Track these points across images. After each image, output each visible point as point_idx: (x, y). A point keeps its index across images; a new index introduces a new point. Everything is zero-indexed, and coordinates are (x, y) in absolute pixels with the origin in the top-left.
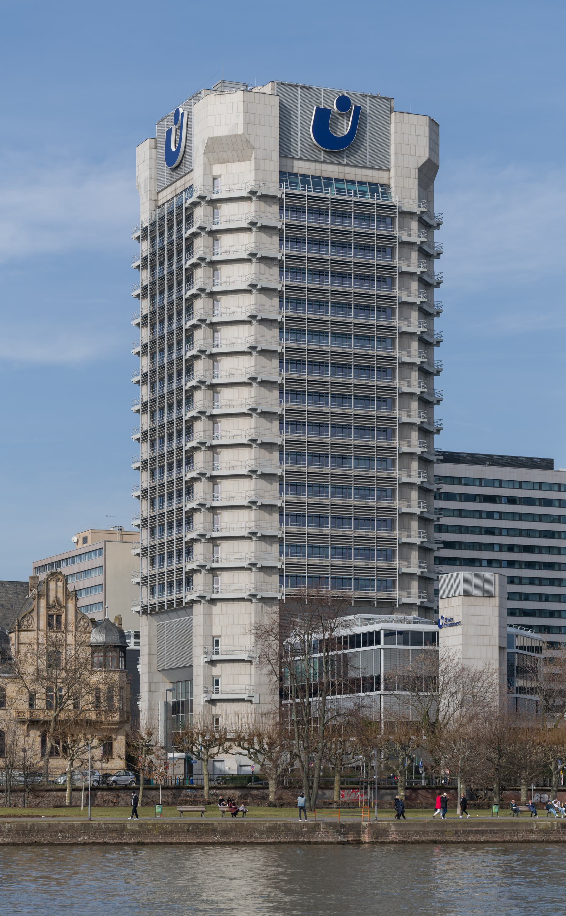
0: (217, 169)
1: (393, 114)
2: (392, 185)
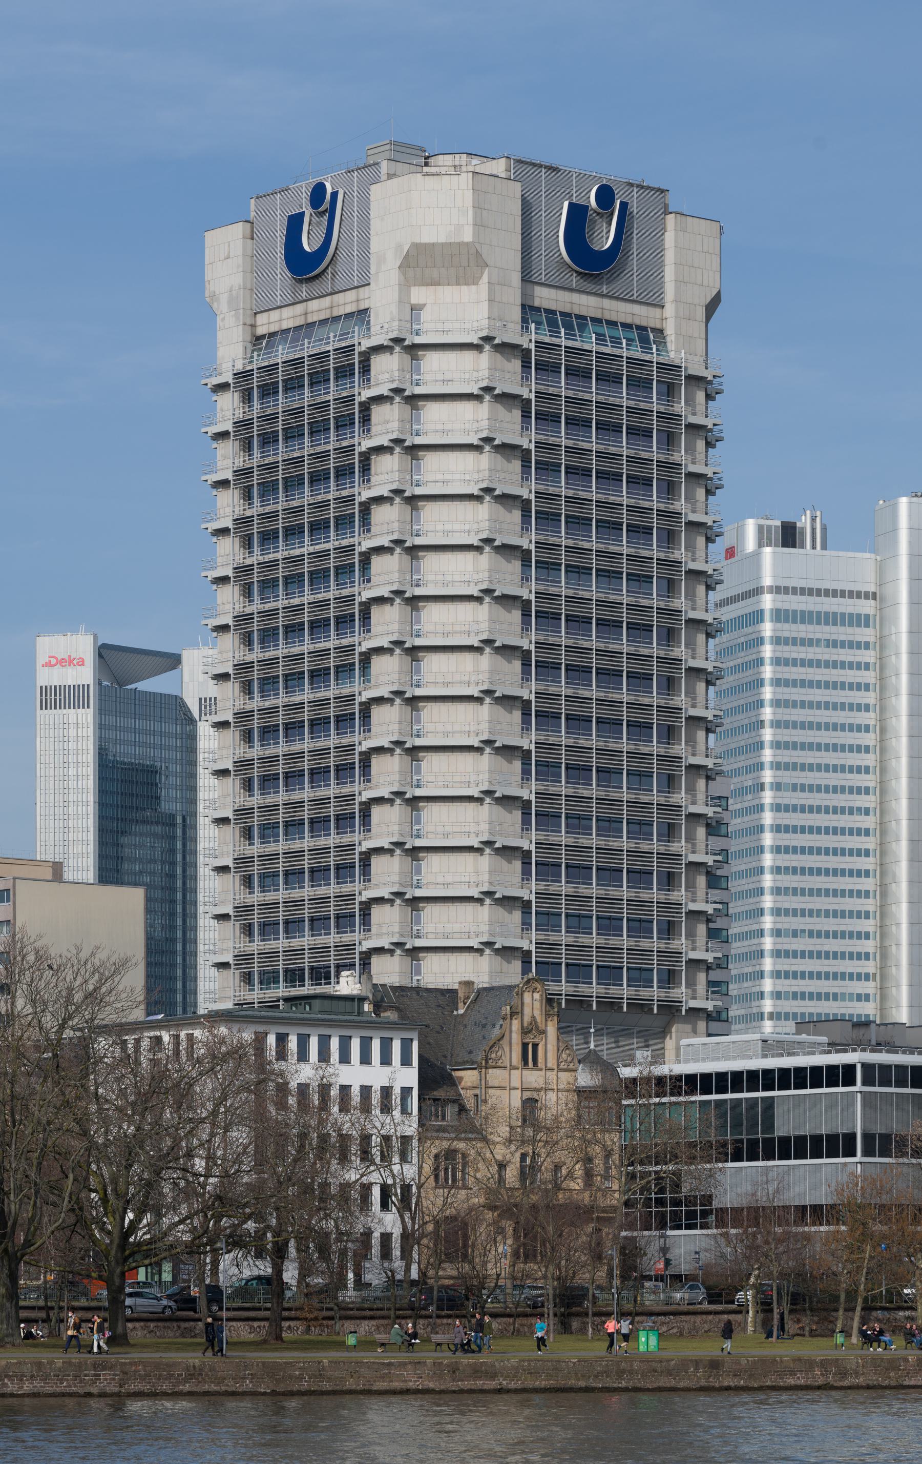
0: (418, 295)
1: (670, 219)
2: (670, 330)
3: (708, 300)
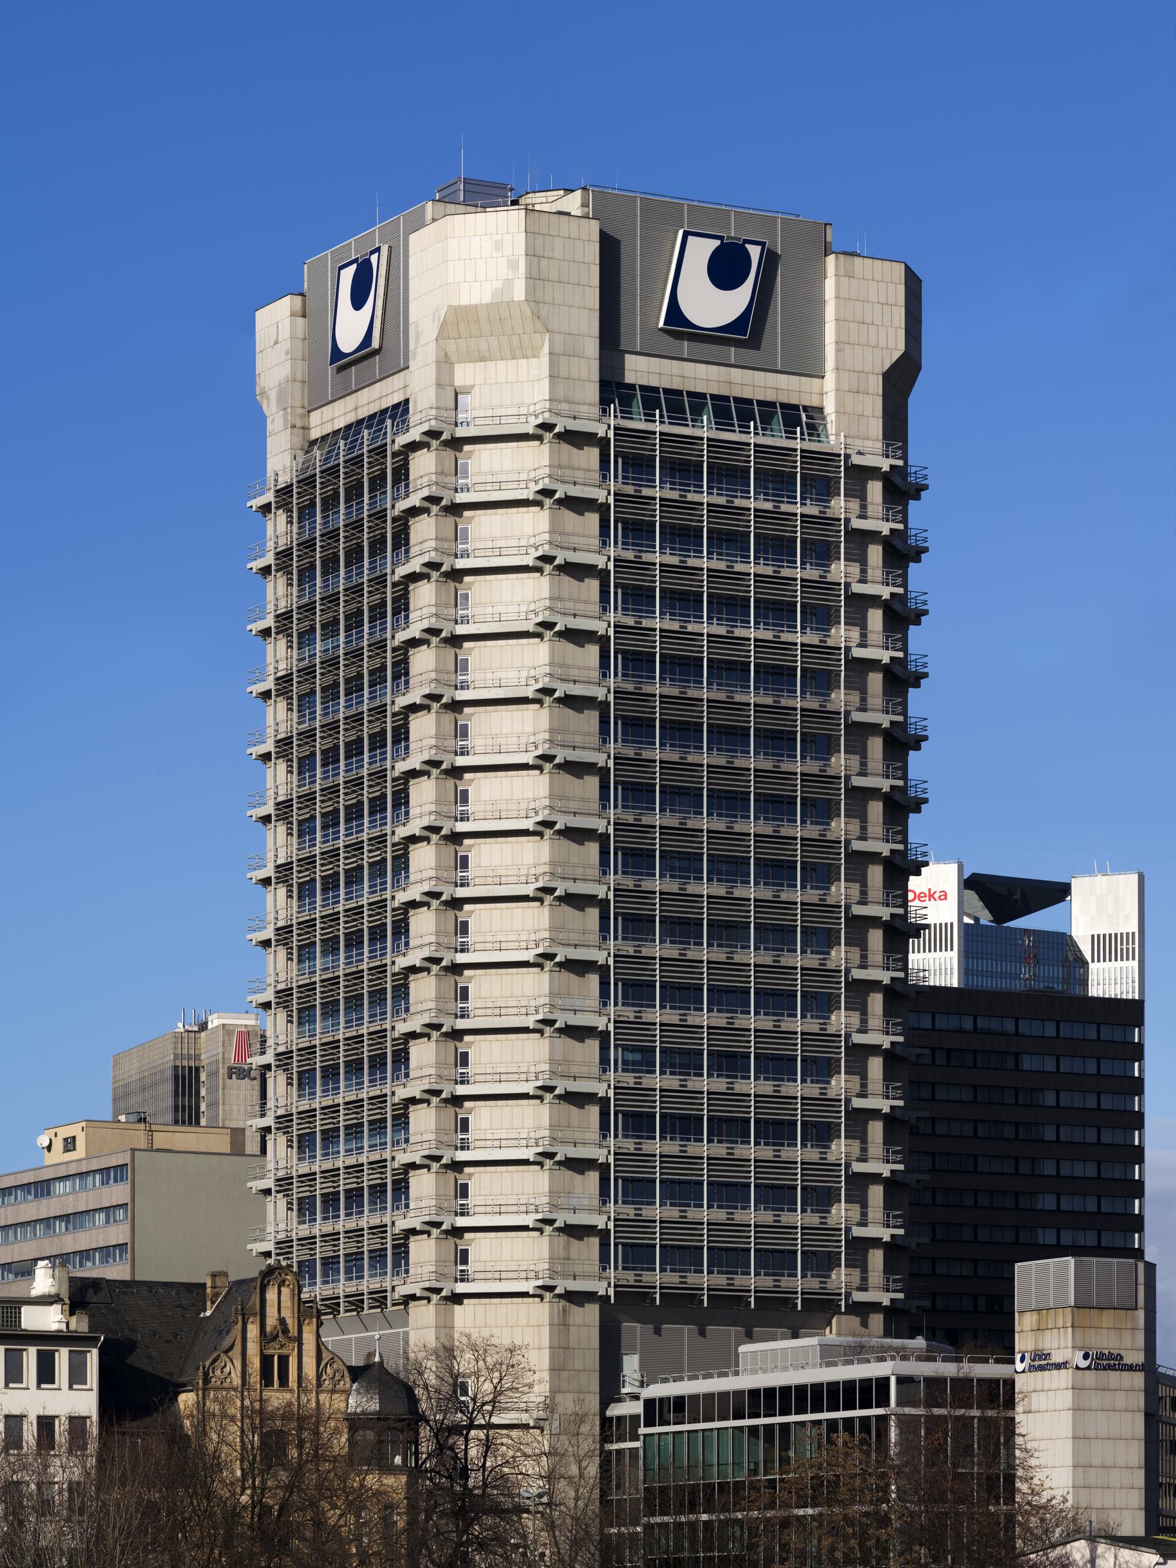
1: (831, 260)
2: (830, 409)
3: (887, 366)
